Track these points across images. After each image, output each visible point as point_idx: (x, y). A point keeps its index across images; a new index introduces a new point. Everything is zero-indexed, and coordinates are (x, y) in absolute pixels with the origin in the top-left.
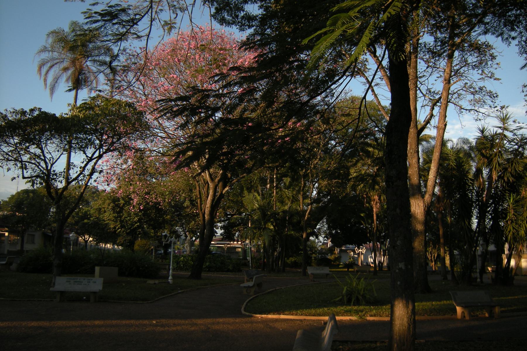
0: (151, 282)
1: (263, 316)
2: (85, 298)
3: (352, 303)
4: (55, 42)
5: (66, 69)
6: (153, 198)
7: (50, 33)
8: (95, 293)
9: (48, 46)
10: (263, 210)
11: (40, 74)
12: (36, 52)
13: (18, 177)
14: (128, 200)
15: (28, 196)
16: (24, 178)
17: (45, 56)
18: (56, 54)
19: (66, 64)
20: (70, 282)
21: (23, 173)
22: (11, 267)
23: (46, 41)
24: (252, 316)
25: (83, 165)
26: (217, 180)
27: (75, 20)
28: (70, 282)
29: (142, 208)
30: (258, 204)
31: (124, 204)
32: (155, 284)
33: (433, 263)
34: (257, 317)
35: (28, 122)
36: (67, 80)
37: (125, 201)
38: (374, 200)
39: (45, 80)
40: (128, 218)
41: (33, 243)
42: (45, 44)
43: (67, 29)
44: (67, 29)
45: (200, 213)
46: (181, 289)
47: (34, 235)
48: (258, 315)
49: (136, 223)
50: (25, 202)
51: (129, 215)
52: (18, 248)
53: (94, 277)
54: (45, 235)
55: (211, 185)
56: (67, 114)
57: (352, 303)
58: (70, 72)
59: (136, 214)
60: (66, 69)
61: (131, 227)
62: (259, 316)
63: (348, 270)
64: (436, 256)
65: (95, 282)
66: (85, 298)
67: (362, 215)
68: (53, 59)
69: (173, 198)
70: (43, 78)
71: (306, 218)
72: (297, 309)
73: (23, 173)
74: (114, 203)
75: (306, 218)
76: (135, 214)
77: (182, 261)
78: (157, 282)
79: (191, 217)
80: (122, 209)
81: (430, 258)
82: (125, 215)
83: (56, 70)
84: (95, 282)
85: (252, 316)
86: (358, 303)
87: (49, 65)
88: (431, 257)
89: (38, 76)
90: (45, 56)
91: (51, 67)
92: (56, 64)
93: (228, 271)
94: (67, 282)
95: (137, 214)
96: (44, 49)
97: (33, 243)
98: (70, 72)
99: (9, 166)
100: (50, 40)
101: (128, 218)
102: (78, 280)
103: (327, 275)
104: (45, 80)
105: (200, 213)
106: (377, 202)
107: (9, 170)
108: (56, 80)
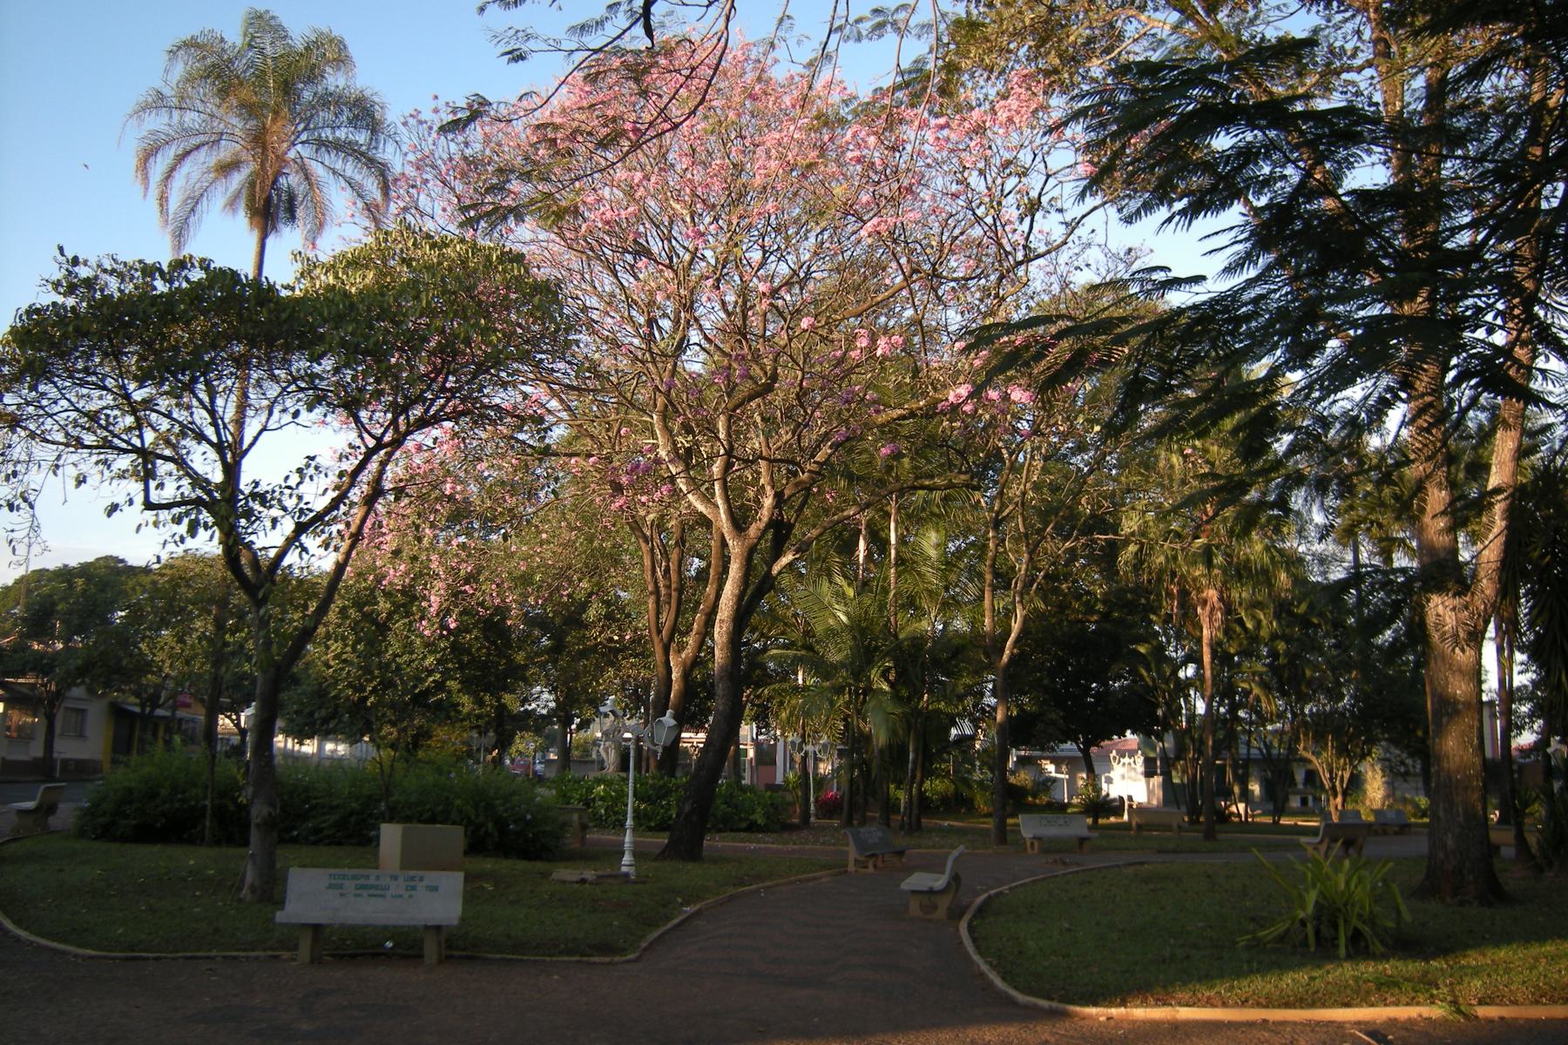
0: (566, 873)
1: (1114, 1011)
2: (389, 944)
3: (1342, 951)
4: (189, 79)
5: (226, 169)
6: (488, 593)
7: (179, 48)
8: (438, 928)
9: (167, 92)
10: (861, 629)
11: (146, 178)
12: (130, 111)
13: (131, 502)
14: (408, 600)
15: (71, 586)
16: (149, 505)
17: (158, 122)
18: (191, 119)
19: (226, 150)
20: (341, 887)
21: (146, 490)
22: (51, 820)
23: (167, 71)
24: (1065, 1015)
25: (349, 466)
26: (753, 531)
27: (261, 9)
28: (341, 887)
29: (453, 626)
30: (847, 614)
31: (390, 615)
32: (583, 881)
33: (1339, 799)
34: (1090, 1017)
35: (168, 309)
36: (232, 204)
37: (393, 604)
38: (1205, 602)
39: (163, 199)
40: (406, 658)
41: (81, 735)
42: (159, 85)
43: (234, 36)
44: (234, 36)
45: (656, 640)
46: (687, 903)
47: (84, 711)
48: (1092, 1011)
49: (430, 673)
50: (59, 607)
51: (408, 648)
52: (37, 750)
53: (375, 864)
54: (118, 713)
55: (736, 548)
56: (293, 289)
57: (1342, 951)
58: (238, 179)
59: (430, 645)
60: (226, 169)
61: (415, 687)
62: (1097, 1013)
63: (1095, 821)
64: (1347, 775)
65: (436, 889)
66: (389, 944)
67: (1142, 650)
68: (187, 132)
69: (551, 594)
70: (154, 192)
71: (1005, 658)
72: (1207, 978)
73: (146, 490)
74: (360, 611)
75: (1005, 658)
76: (427, 645)
77: (602, 799)
78: (589, 874)
79: (603, 654)
80: (383, 628)
81: (1327, 785)
82: (396, 647)
83: (193, 171)
84: (436, 889)
85: (1065, 1015)
86: (1359, 948)
87: (171, 152)
88: (1331, 779)
89: (139, 188)
90: (158, 122)
91: (182, 157)
92: (197, 147)
93: (752, 828)
94: (331, 886)
95: (433, 644)
96: (158, 102)
97: (81, 735)
98: (238, 179)
99: (84, 468)
100: (179, 70)
101: (406, 658)
102: (372, 881)
103: (1082, 840)
104: (163, 199)
105: (656, 640)
106: (1213, 609)
107: (81, 481)
108: (193, 203)
